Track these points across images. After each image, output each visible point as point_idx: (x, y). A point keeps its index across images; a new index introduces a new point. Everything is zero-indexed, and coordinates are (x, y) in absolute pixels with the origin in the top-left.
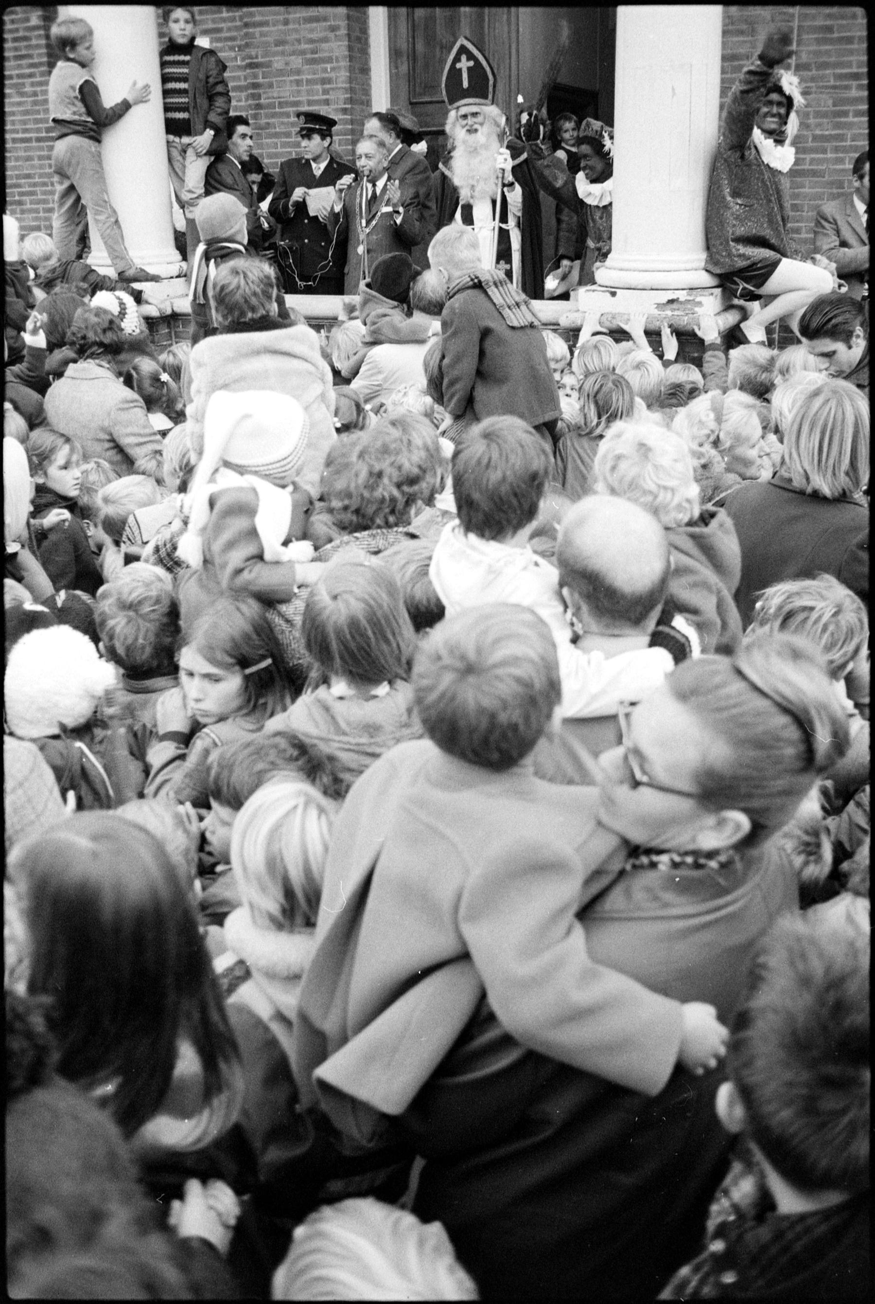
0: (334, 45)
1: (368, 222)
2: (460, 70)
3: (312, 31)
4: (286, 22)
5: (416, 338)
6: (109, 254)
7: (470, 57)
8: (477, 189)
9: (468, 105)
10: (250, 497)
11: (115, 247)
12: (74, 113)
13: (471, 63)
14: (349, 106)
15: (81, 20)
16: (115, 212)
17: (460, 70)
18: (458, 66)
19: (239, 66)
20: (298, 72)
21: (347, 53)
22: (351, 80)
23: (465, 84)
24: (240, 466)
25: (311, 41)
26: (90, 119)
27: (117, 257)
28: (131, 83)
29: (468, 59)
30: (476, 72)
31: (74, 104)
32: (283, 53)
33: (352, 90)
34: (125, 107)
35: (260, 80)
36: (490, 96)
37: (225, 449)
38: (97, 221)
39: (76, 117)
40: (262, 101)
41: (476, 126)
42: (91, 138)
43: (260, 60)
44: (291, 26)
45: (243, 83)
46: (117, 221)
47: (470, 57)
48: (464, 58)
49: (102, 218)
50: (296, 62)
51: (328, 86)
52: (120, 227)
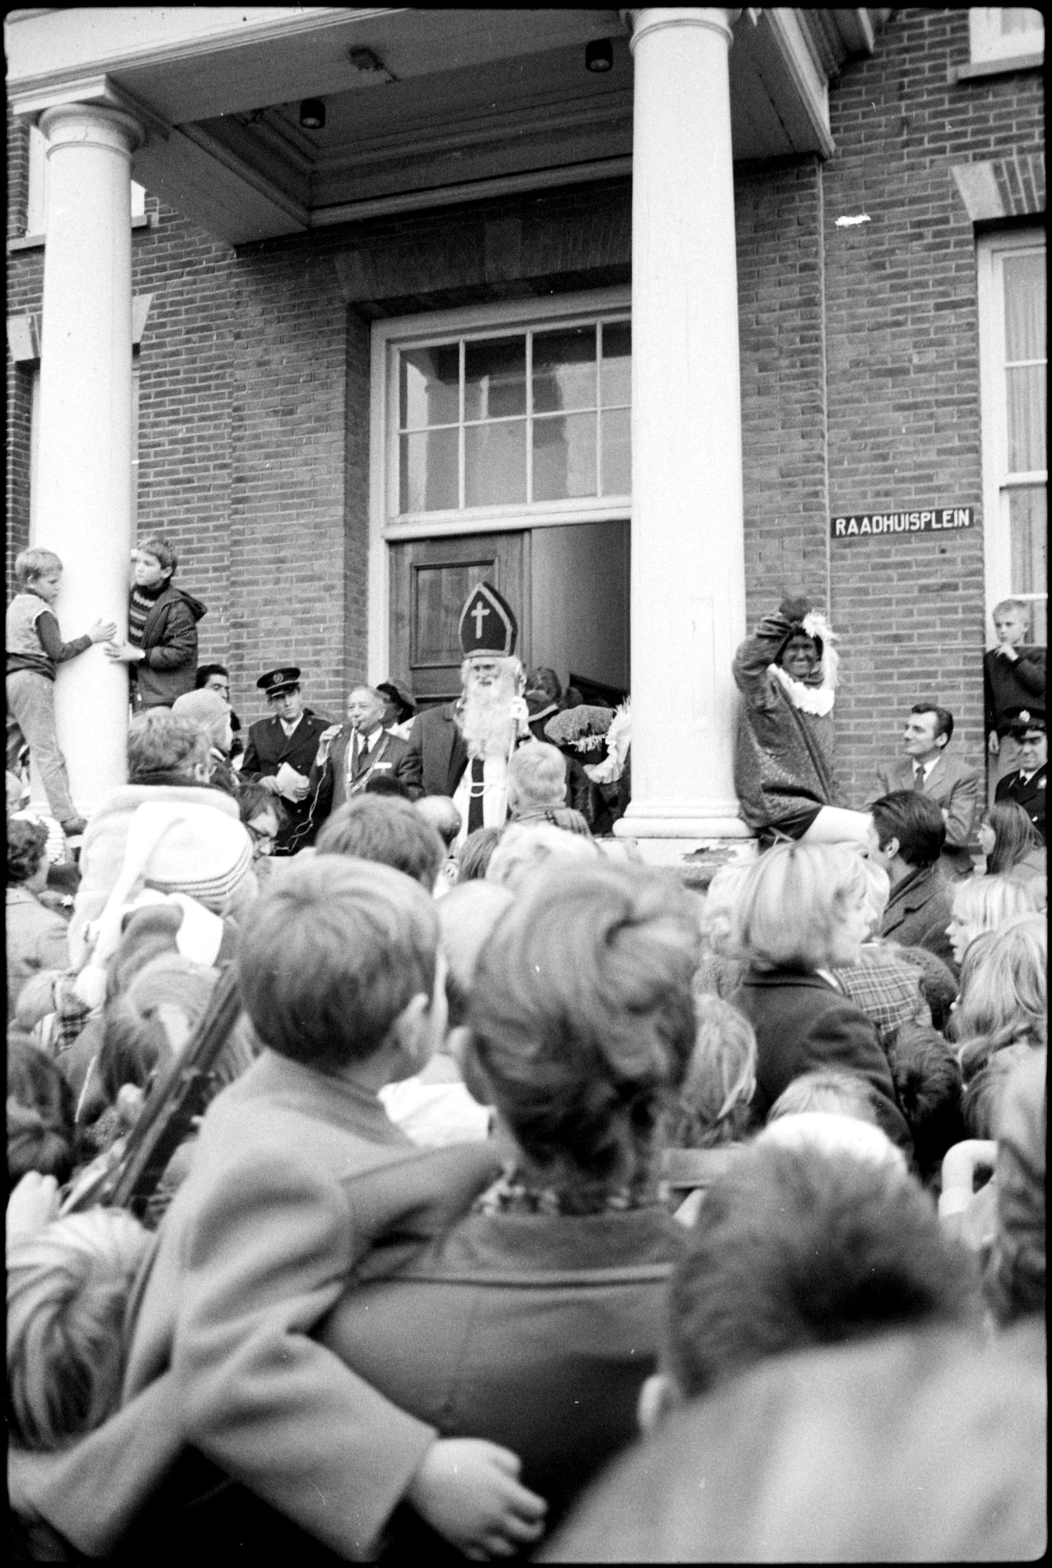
0: (328, 605)
1: (356, 779)
2: (475, 618)
3: (304, 590)
4: (277, 582)
5: (454, 570)
6: (50, 801)
7: (487, 605)
8: (489, 743)
9: (482, 656)
10: (176, 914)
11: (60, 795)
12: (27, 647)
13: (487, 612)
14: (341, 668)
15: (53, 555)
16: (61, 755)
17: (475, 618)
18: (474, 613)
19: (222, 627)
20: (287, 632)
21: (342, 613)
22: (345, 640)
23: (479, 634)
24: (166, 884)
25: (302, 601)
26: (44, 654)
27: (58, 805)
28: (96, 621)
29: (484, 607)
30: (493, 622)
31: (28, 637)
32: (271, 613)
33: (346, 651)
34: (86, 643)
35: (244, 640)
36: (508, 647)
37: (148, 863)
38: (39, 764)
39: (29, 651)
40: (245, 662)
41: (489, 679)
42: (45, 674)
43: (245, 619)
44: (282, 585)
45: (225, 644)
46: (63, 766)
47: (487, 605)
48: (480, 605)
49: (46, 760)
50: (286, 622)
51: (319, 647)
52: (65, 772)
